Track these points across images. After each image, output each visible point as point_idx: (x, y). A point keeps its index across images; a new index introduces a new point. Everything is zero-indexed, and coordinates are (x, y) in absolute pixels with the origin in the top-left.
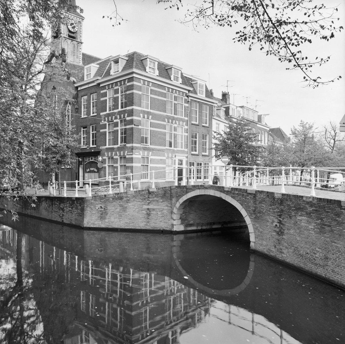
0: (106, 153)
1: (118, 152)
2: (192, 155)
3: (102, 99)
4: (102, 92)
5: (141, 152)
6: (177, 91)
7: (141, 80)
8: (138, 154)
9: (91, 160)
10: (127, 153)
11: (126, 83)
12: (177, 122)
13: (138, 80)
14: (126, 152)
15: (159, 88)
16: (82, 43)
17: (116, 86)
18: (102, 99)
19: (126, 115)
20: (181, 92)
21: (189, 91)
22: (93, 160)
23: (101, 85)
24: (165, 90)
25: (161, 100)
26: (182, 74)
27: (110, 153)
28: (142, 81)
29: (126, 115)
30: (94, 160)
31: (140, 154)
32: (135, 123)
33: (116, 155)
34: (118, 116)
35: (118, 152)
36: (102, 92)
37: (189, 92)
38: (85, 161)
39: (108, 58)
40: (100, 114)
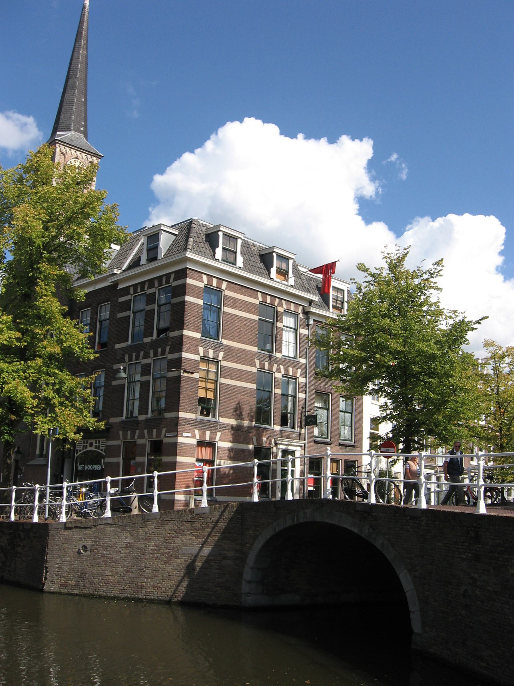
0: (121, 433)
1: (146, 431)
2: (315, 442)
3: (120, 315)
4: (121, 300)
5: (197, 431)
6: (284, 302)
7: (283, 301)
8: (189, 435)
9: (89, 448)
10: (167, 432)
11: (171, 281)
12: (282, 367)
13: (196, 275)
14: (164, 430)
15: (242, 294)
16: (191, 223)
17: (150, 287)
18: (120, 315)
19: (168, 348)
20: (292, 304)
21: (310, 302)
22: (93, 448)
23: (120, 287)
24: (257, 298)
25: (247, 319)
26: (295, 266)
27: (129, 432)
28: (260, 294)
29: (168, 348)
30: (96, 448)
31: (194, 436)
32: (184, 366)
33: (141, 436)
34: (151, 352)
35: (146, 431)
36: (121, 300)
37: (310, 305)
38: (77, 450)
39: (317, 278)
40: (114, 347)
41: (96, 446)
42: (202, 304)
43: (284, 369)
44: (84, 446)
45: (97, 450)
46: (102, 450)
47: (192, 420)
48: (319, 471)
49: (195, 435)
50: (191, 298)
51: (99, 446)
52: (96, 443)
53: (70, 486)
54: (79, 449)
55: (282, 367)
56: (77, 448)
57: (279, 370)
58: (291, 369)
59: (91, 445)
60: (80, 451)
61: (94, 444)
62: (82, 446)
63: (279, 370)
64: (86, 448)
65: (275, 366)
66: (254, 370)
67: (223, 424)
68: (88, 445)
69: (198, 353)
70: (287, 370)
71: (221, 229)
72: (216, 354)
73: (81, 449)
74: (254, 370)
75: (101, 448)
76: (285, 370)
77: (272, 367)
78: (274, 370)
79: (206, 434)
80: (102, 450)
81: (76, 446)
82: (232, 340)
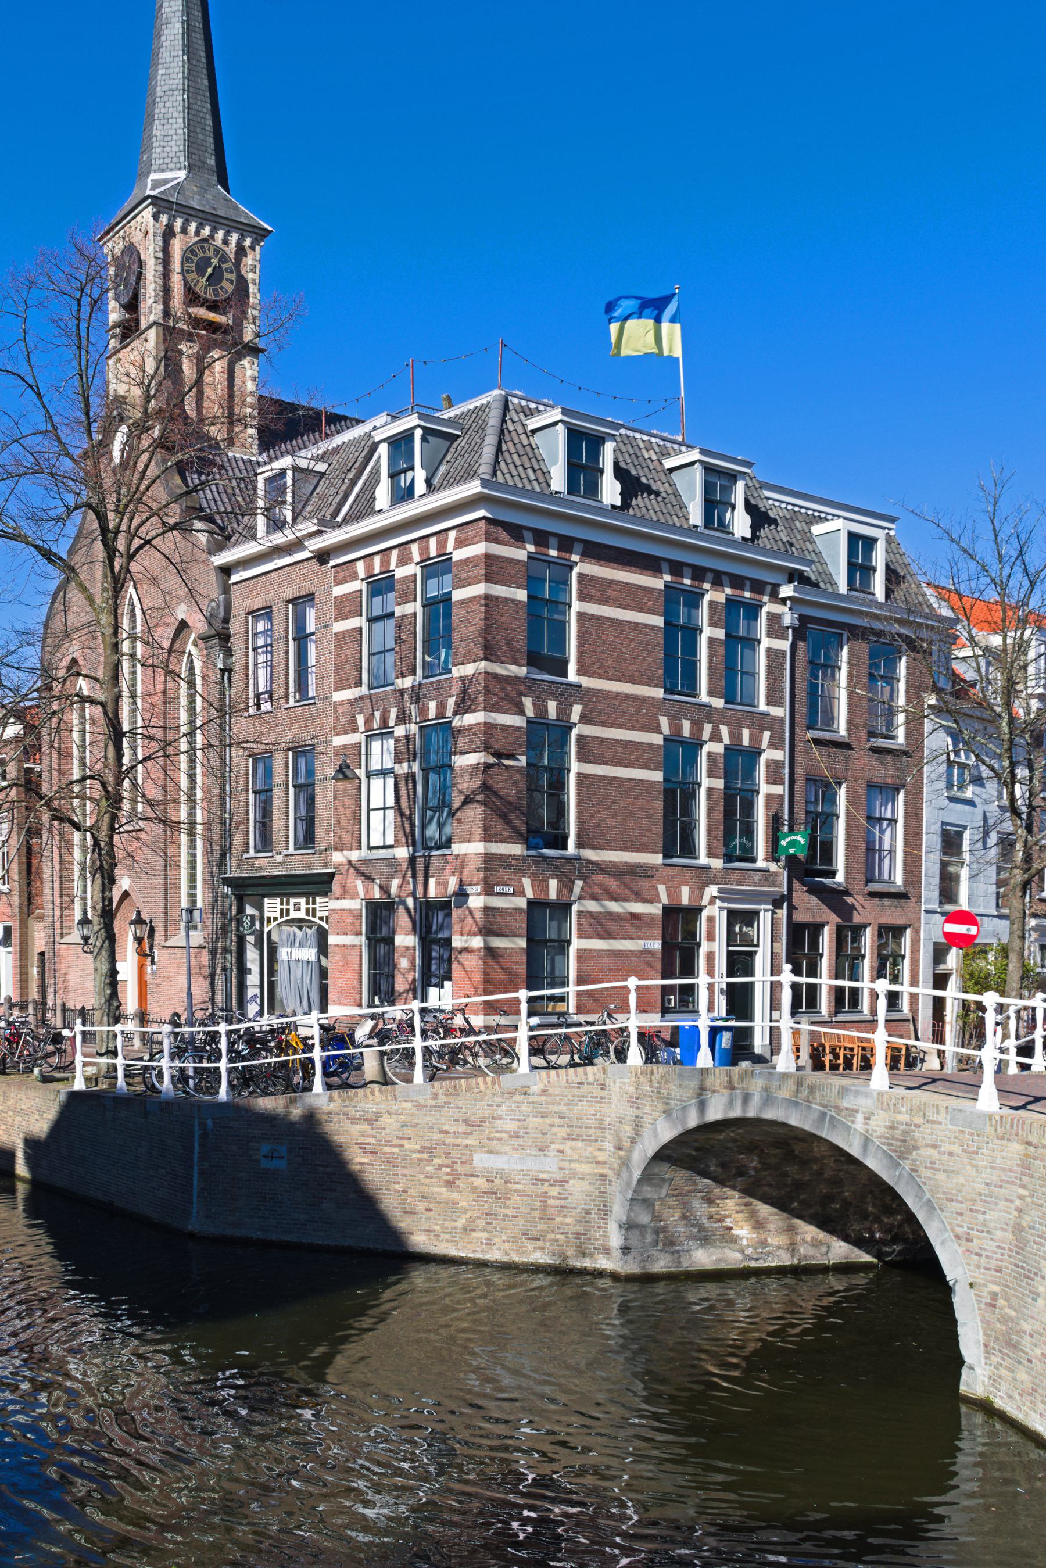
5: (526, 882)
12: (724, 730)
30: (307, 914)
38: (269, 919)
41: (307, 910)
42: (525, 599)
43: (730, 733)
44: (282, 910)
45: (310, 918)
46: (321, 918)
47: (515, 857)
48: (831, 865)
49: (524, 890)
50: (499, 587)
51: (314, 910)
52: (308, 903)
53: (160, 1075)
54: (272, 915)
55: (724, 730)
56: (267, 914)
57: (716, 737)
58: (746, 733)
59: (298, 909)
60: (275, 919)
61: (303, 906)
62: (278, 910)
63: (716, 737)
64: (288, 914)
65: (708, 728)
66: (658, 740)
67: (589, 861)
68: (291, 907)
69: (521, 711)
70: (735, 736)
71: (377, 439)
72: (564, 711)
73: (278, 914)
74: (658, 740)
75: (319, 914)
76: (731, 735)
77: (701, 730)
78: (706, 735)
79: (547, 886)
80: (321, 918)
81: (266, 909)
82: (600, 677)
